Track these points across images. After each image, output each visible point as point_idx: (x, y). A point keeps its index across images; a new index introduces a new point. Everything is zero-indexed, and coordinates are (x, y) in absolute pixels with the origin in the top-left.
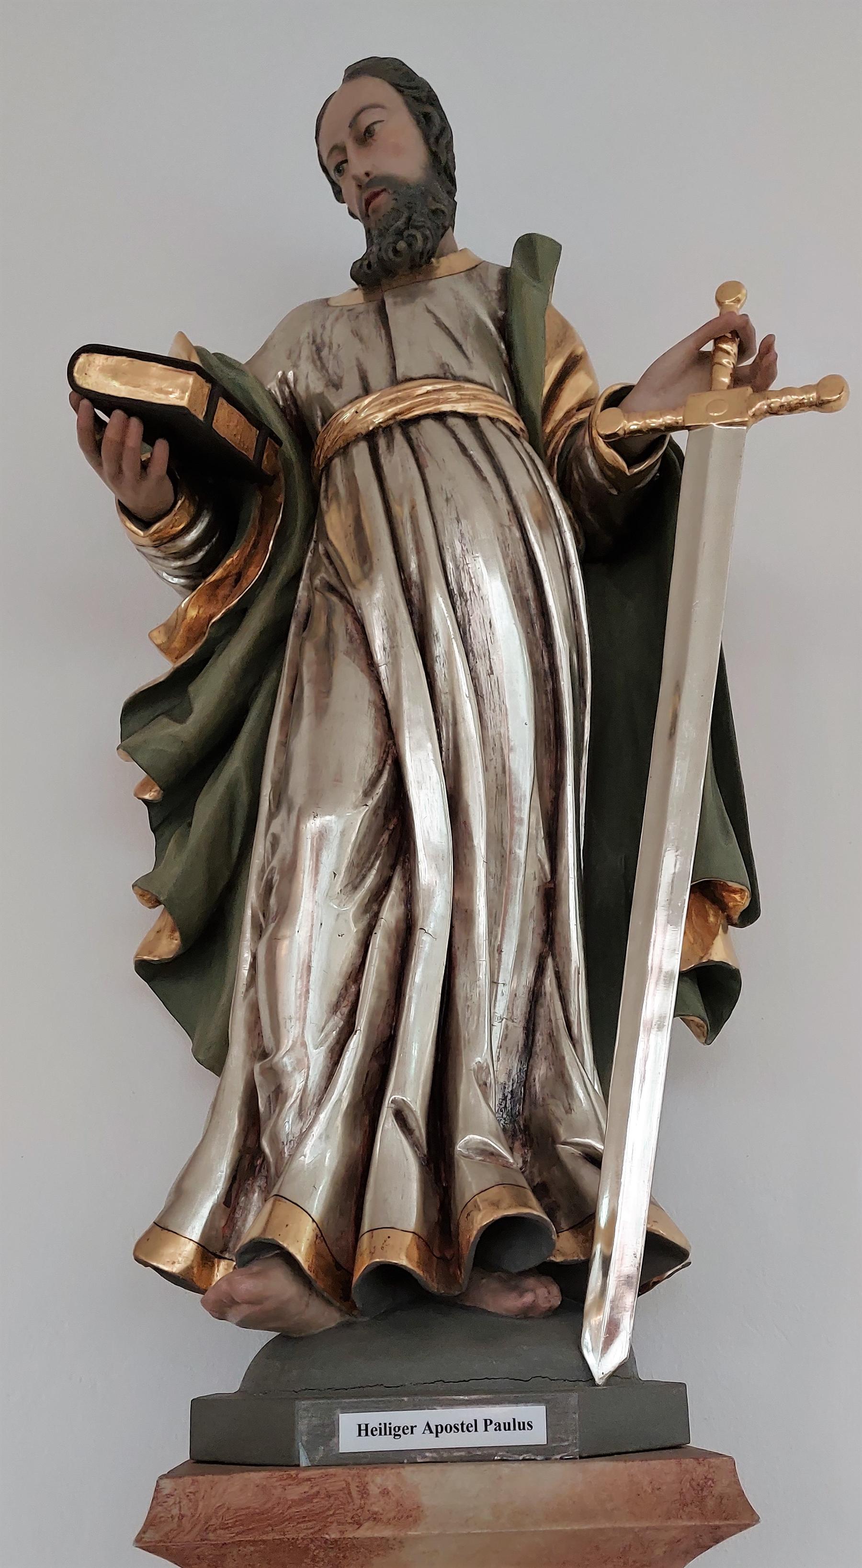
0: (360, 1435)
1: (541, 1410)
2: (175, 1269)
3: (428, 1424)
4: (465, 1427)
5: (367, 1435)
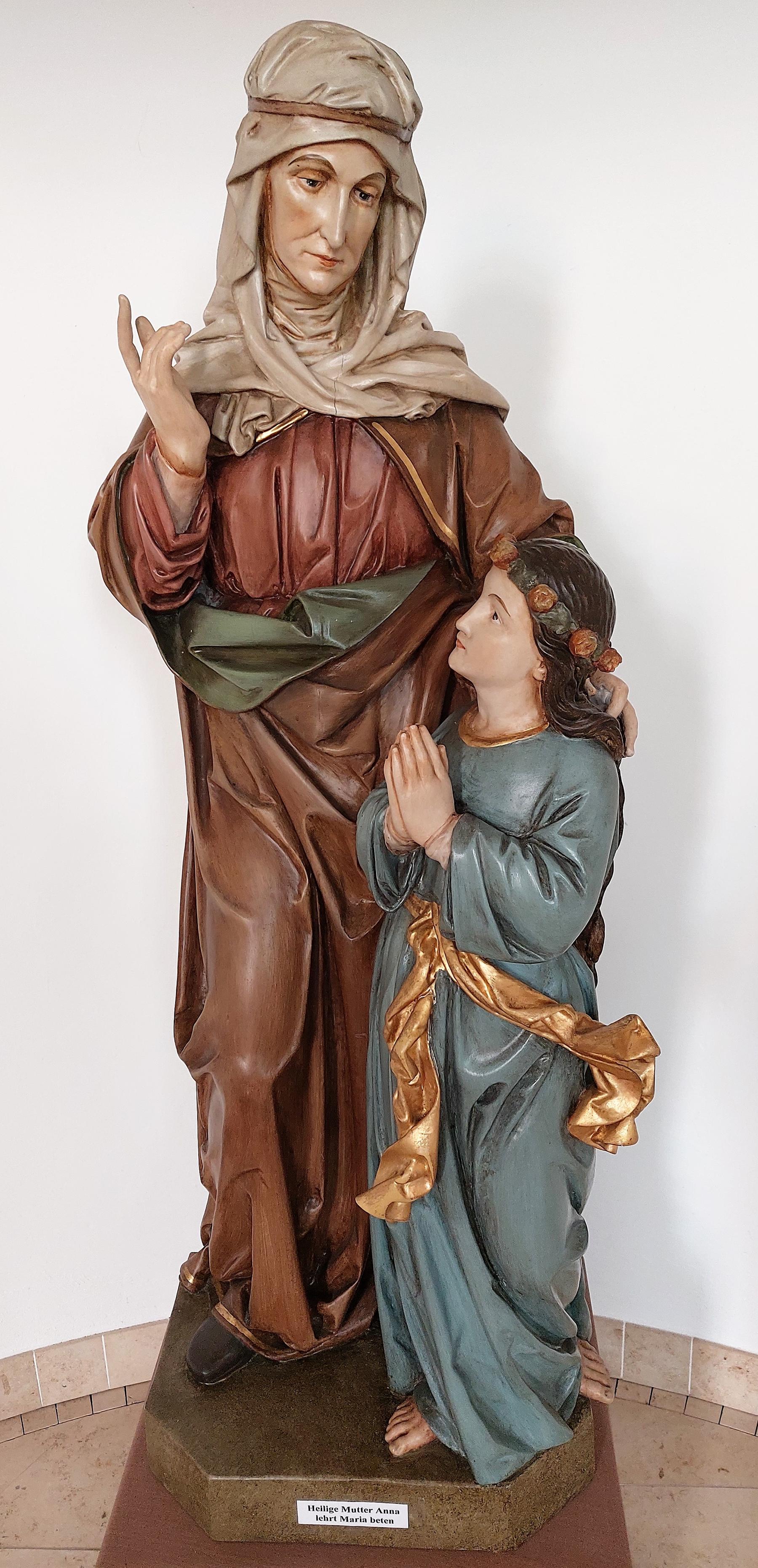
0: (309, 1510)
1: (301, 1521)
2: (624, 1141)
3: (379, 1509)
4: (383, 1521)
5: (313, 1510)
